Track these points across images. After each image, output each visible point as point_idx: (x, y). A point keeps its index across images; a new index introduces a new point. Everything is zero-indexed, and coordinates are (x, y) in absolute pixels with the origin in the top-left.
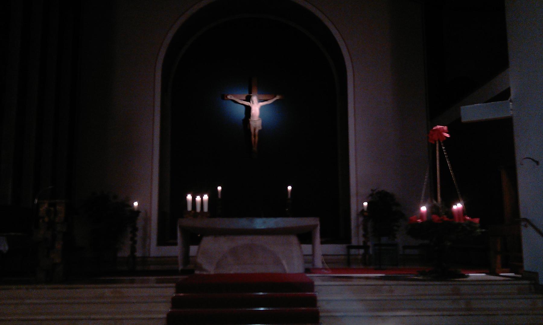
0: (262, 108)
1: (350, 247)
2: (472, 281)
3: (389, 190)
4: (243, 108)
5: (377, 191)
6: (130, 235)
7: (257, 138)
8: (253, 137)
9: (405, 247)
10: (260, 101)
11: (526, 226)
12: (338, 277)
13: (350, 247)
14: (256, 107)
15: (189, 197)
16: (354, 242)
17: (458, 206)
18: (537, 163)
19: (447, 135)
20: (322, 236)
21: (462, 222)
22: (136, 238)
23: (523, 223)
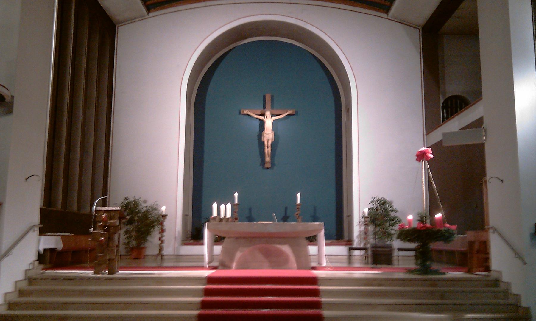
0: (274, 122)
1: (351, 249)
2: (449, 278)
3: (388, 198)
4: (258, 123)
5: (377, 198)
6: (159, 236)
7: (270, 149)
8: (266, 147)
9: (399, 250)
10: (273, 115)
11: (494, 232)
12: (73, 68)
13: (351, 249)
14: (269, 122)
15: (215, 206)
16: (355, 244)
17: (438, 216)
18: (502, 181)
19: (432, 156)
20: (326, 238)
21: (443, 229)
22: (163, 239)
23: (491, 231)
